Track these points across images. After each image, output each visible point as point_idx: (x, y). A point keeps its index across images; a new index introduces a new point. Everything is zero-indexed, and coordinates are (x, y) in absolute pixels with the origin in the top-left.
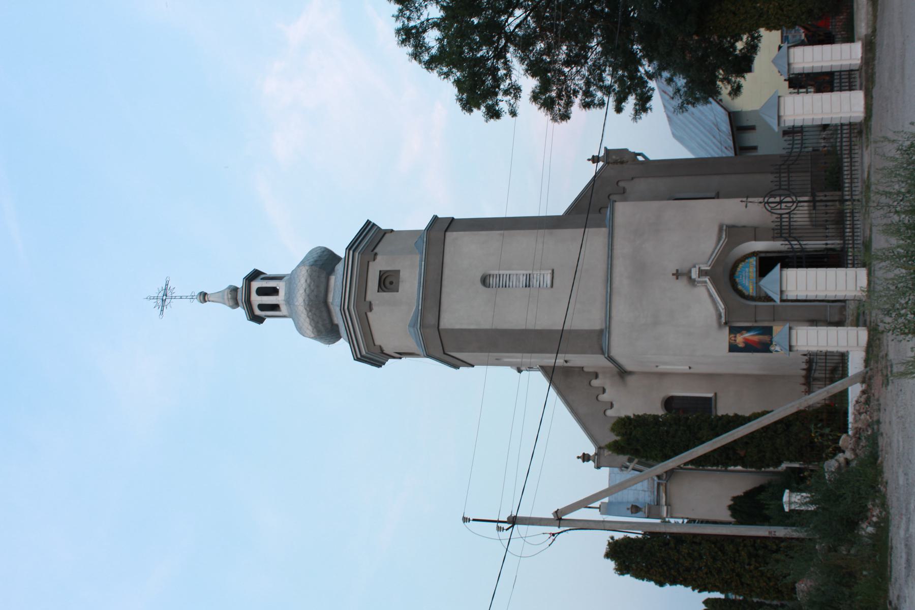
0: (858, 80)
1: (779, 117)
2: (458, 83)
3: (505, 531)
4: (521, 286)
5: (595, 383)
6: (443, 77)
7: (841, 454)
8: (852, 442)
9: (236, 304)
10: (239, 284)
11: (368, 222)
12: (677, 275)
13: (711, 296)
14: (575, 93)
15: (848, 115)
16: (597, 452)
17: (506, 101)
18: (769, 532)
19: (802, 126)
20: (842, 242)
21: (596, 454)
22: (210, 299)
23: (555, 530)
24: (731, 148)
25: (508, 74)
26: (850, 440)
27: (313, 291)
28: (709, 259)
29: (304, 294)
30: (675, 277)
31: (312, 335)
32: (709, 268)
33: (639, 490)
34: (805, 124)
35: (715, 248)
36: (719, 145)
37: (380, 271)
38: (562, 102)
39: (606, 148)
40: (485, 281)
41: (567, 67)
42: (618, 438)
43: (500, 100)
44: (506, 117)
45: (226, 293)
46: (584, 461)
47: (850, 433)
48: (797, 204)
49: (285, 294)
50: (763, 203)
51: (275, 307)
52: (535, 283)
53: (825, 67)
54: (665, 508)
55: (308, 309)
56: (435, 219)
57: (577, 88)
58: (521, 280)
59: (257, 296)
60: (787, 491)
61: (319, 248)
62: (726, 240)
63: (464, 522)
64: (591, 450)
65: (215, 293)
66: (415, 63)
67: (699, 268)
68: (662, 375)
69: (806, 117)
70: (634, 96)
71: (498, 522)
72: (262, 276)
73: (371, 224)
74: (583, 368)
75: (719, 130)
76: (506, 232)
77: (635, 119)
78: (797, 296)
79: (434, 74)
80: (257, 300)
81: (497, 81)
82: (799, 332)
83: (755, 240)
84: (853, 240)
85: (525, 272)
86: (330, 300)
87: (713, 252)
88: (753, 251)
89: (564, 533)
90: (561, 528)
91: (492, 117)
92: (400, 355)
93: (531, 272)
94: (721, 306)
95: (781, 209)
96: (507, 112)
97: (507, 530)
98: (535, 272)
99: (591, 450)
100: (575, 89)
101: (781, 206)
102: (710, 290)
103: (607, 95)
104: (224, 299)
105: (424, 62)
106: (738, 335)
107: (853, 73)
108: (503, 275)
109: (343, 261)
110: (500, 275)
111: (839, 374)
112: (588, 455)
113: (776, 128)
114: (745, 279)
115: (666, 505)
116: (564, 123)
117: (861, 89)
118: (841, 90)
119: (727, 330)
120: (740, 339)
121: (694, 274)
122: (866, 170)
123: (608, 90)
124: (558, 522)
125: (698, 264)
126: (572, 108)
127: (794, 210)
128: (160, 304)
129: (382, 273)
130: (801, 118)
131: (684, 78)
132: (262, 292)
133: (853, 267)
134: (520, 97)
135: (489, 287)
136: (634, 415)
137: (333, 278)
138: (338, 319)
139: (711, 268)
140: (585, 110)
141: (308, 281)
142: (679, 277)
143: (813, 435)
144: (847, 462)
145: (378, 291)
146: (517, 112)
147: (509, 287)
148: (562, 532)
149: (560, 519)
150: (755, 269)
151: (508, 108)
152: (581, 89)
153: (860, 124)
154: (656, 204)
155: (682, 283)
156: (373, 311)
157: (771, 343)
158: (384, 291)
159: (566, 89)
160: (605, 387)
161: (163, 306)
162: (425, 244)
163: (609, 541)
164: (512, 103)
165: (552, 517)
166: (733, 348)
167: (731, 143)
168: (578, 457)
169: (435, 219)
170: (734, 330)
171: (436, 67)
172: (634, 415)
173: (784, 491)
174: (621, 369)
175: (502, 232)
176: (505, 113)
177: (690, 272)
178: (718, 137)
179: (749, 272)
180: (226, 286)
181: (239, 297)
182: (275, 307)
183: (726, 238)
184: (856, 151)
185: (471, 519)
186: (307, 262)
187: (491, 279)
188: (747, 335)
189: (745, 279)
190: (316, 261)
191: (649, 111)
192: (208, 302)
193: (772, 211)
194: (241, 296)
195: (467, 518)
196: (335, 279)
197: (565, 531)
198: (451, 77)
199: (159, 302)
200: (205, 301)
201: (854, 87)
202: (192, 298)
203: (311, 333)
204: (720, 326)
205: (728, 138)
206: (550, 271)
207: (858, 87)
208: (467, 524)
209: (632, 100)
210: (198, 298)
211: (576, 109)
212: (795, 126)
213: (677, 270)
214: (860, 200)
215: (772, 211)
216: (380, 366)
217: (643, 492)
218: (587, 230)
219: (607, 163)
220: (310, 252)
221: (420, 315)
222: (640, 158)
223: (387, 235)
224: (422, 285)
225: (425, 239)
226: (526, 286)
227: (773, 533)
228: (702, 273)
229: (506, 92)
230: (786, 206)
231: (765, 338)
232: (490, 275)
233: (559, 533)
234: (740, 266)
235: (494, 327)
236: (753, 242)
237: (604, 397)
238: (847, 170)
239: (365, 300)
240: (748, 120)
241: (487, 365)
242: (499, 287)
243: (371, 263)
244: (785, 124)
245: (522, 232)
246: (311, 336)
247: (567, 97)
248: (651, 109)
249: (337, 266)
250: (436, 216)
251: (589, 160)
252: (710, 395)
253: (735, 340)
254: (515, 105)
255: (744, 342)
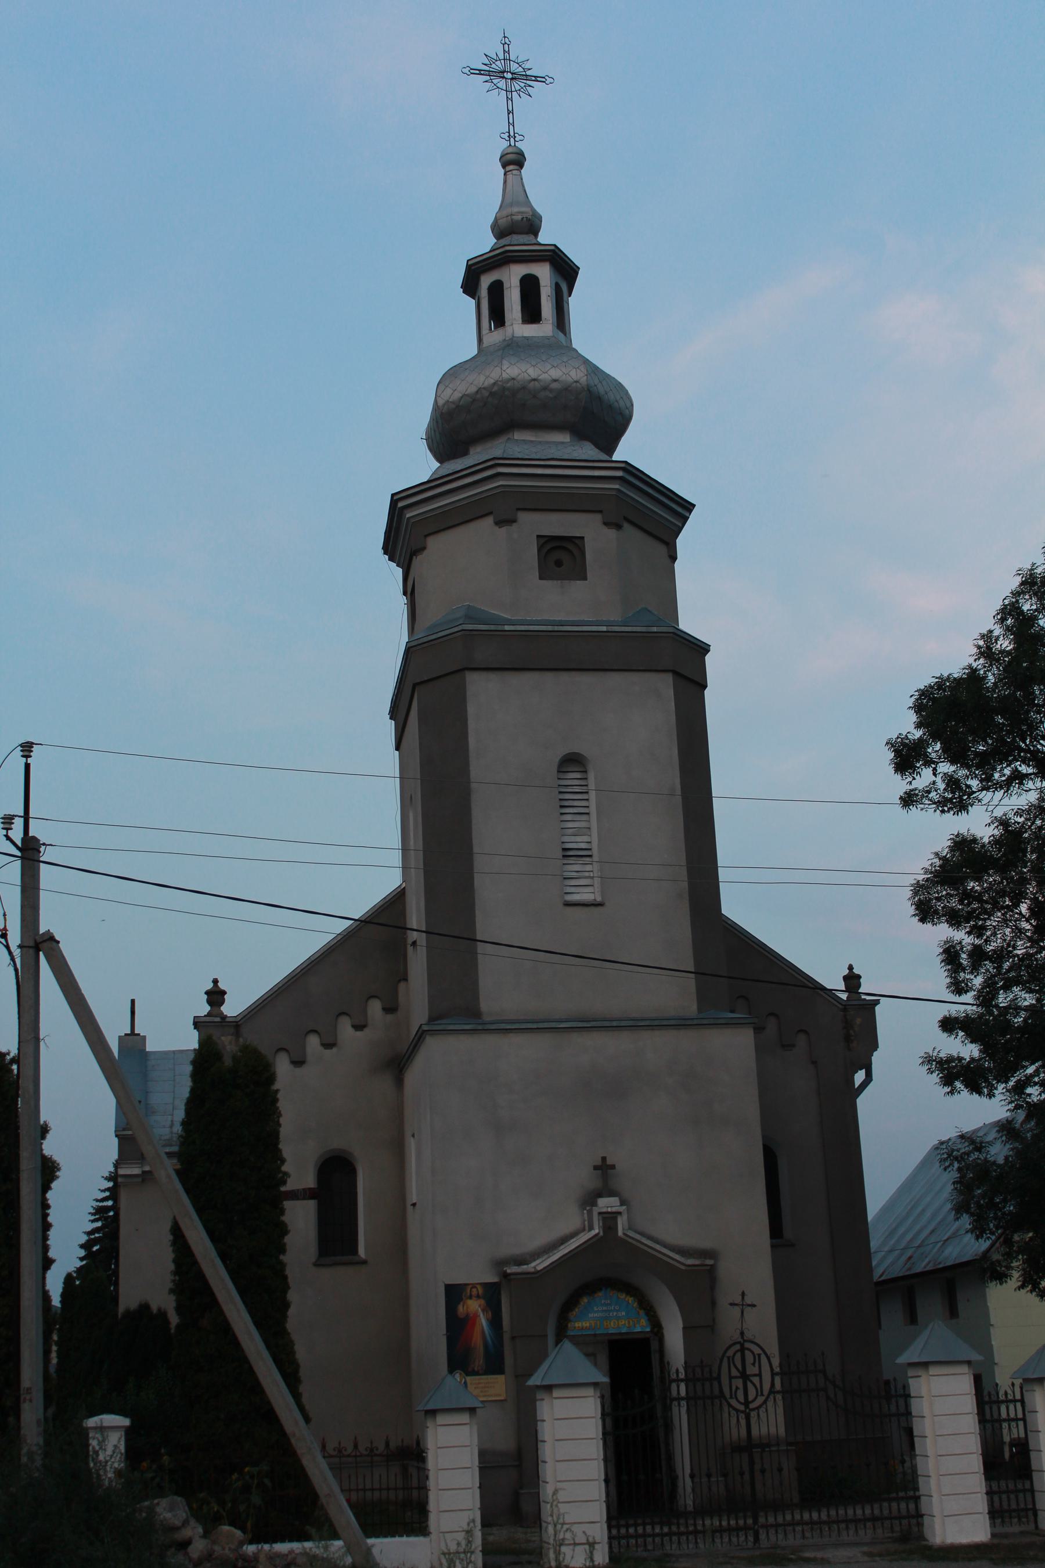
0: (1016, 1529)
1: (925, 1365)
2: (973, 677)
3: (4, 832)
4: (566, 839)
5: (375, 1007)
6: (981, 643)
7: (200, 1530)
8: (227, 1551)
9: (501, 231)
10: (545, 237)
11: (689, 507)
12: (604, 1168)
13: (564, 1240)
14: (978, 931)
15: (936, 1511)
16: (228, 1020)
17: (934, 783)
18: (30, 1388)
19: (910, 1413)
20: (690, 1508)
21: (224, 1017)
22: (510, 176)
23: (15, 938)
24: (909, 1269)
25: (988, 784)
26: (230, 1549)
27: (534, 397)
28: (642, 1234)
29: (527, 378)
30: (599, 1163)
31: (441, 402)
32: (620, 1233)
33: (172, 1115)
34: (914, 1419)
35: (665, 1246)
36: (918, 1242)
37: (582, 538)
38: (954, 903)
39: (877, 1002)
40: (573, 761)
41: (1029, 909)
42: (228, 1062)
43: (935, 769)
44: (900, 785)
45: (523, 209)
46: (207, 993)
47: (251, 1549)
48: (742, 1412)
49: (527, 338)
50: (740, 1340)
51: (498, 316)
52: (574, 867)
53: (1040, 1459)
54: (136, 1171)
55: (495, 388)
56: (703, 649)
57: (989, 933)
58: (578, 839)
59: (519, 277)
60: (126, 1422)
61: (628, 405)
62: (683, 1268)
63: (21, 745)
64: (232, 1008)
65: (523, 186)
66: (1015, 582)
67: (620, 1213)
68: (398, 1147)
69: (927, 1422)
70: (976, 1054)
71: (26, 817)
72: (564, 287)
73: (687, 514)
74: (406, 980)
75: (948, 1239)
76: (678, 800)
77: (928, 1060)
78: (544, 1421)
79: (988, 622)
80: (512, 277)
81: (985, 764)
82: (467, 1428)
83: (684, 1328)
84: (688, 1533)
85: (595, 846)
86: (518, 435)
87: (657, 1242)
88: (664, 1324)
89: (8, 958)
90: (19, 950)
91: (898, 753)
92: (410, 591)
93: (596, 858)
94: (541, 1264)
95: (731, 1378)
96: (911, 787)
97: (8, 838)
98: (596, 866)
99: (232, 1008)
100: (986, 930)
101: (736, 1377)
102: (574, 1239)
103: (977, 998)
104: (511, 205)
105: (1017, 601)
106: (482, 1302)
107: (1032, 1518)
108: (587, 800)
109: (605, 457)
110: (587, 793)
111: (909, 1524)
112: (222, 1002)
113: (902, 1360)
114: (603, 1311)
115: (144, 1172)
116: (912, 910)
117: (993, 1535)
118: (990, 1493)
119: (492, 1278)
120: (473, 1306)
121: (607, 1204)
122: (819, 1555)
123: (986, 998)
124: (32, 944)
125: (628, 1210)
126: (946, 925)
127: (730, 1405)
128: (493, 66)
129: (577, 541)
130: (926, 1412)
131: (1006, 1158)
132: (530, 287)
133: (610, 1538)
134: (943, 811)
135: (558, 772)
136: (277, 1091)
137: (565, 438)
138: (477, 455)
139: (621, 1238)
140: (941, 954)
141: (554, 385)
142: (599, 1172)
143: (247, 1469)
144: (184, 1545)
145: (538, 536)
146: (913, 809)
147: (562, 814)
148: (10, 953)
149: (37, 948)
150: (624, 1330)
151: (921, 788)
152: (986, 941)
153: (921, 1537)
154: (752, 1112)
155: (584, 1177)
156: (497, 528)
157: (468, 1373)
158: (539, 550)
159: (985, 912)
160: (366, 1030)
161: (489, 73)
162: (644, 629)
163: (8, 1054)
164: (933, 794)
165: (42, 931)
166: (454, 1293)
167: (919, 1268)
168: (215, 982)
169: (703, 649)
170: (491, 1294)
171: (1008, 629)
172: (277, 1091)
173: (125, 1415)
174: (404, 1060)
175: (679, 792)
176: (911, 783)
177: (612, 1194)
178: (932, 1239)
179: (618, 1318)
180: (539, 209)
181: (516, 238)
182: (498, 316)
183: (689, 1266)
184: (879, 1531)
185: (30, 760)
186: (596, 381)
187: (578, 775)
188: (483, 1321)
189: (603, 1311)
190: (599, 398)
191: (947, 1089)
192: (502, 171)
193: (725, 1360)
194: (518, 242)
195: (32, 751)
196: (563, 443)
197: (13, 959)
198: (982, 661)
199: (498, 63)
200: (504, 166)
201: (998, 1521)
202: (509, 137)
203: (446, 398)
204: (499, 1264)
205: (929, 1262)
206: (599, 899)
207: (999, 1530)
208: (18, 752)
209: (970, 1051)
210: (510, 150)
211: (943, 932)
212: (908, 1399)
213: (613, 1167)
214: (757, 1545)
215: (725, 1360)
216: (386, 549)
217: (169, 1123)
218: (693, 976)
219: (845, 1006)
220: (620, 387)
221: (493, 627)
222: (860, 1077)
223: (662, 549)
224: (556, 628)
225: (655, 629)
226: (564, 850)
227: (28, 1397)
228: (609, 1220)
229: (952, 783)
230: (737, 1388)
231: (479, 1361)
232: (586, 772)
233: (7, 947)
234: (631, 1300)
235: (473, 786)
236: (681, 1325)
237: (345, 1028)
238: (872, 1510)
239: (518, 509)
240: (968, 1301)
241: (402, 778)
242: (560, 792)
243: (598, 517)
244: (912, 1377)
245: (681, 835)
246: (439, 399)
247: (968, 912)
248: (952, 1092)
249: (590, 444)
250: (709, 651)
251: (851, 968)
252: (362, 1252)
253: (471, 1297)
254: (927, 802)
255: (467, 1315)
